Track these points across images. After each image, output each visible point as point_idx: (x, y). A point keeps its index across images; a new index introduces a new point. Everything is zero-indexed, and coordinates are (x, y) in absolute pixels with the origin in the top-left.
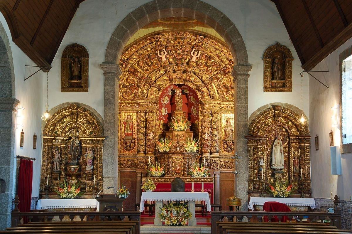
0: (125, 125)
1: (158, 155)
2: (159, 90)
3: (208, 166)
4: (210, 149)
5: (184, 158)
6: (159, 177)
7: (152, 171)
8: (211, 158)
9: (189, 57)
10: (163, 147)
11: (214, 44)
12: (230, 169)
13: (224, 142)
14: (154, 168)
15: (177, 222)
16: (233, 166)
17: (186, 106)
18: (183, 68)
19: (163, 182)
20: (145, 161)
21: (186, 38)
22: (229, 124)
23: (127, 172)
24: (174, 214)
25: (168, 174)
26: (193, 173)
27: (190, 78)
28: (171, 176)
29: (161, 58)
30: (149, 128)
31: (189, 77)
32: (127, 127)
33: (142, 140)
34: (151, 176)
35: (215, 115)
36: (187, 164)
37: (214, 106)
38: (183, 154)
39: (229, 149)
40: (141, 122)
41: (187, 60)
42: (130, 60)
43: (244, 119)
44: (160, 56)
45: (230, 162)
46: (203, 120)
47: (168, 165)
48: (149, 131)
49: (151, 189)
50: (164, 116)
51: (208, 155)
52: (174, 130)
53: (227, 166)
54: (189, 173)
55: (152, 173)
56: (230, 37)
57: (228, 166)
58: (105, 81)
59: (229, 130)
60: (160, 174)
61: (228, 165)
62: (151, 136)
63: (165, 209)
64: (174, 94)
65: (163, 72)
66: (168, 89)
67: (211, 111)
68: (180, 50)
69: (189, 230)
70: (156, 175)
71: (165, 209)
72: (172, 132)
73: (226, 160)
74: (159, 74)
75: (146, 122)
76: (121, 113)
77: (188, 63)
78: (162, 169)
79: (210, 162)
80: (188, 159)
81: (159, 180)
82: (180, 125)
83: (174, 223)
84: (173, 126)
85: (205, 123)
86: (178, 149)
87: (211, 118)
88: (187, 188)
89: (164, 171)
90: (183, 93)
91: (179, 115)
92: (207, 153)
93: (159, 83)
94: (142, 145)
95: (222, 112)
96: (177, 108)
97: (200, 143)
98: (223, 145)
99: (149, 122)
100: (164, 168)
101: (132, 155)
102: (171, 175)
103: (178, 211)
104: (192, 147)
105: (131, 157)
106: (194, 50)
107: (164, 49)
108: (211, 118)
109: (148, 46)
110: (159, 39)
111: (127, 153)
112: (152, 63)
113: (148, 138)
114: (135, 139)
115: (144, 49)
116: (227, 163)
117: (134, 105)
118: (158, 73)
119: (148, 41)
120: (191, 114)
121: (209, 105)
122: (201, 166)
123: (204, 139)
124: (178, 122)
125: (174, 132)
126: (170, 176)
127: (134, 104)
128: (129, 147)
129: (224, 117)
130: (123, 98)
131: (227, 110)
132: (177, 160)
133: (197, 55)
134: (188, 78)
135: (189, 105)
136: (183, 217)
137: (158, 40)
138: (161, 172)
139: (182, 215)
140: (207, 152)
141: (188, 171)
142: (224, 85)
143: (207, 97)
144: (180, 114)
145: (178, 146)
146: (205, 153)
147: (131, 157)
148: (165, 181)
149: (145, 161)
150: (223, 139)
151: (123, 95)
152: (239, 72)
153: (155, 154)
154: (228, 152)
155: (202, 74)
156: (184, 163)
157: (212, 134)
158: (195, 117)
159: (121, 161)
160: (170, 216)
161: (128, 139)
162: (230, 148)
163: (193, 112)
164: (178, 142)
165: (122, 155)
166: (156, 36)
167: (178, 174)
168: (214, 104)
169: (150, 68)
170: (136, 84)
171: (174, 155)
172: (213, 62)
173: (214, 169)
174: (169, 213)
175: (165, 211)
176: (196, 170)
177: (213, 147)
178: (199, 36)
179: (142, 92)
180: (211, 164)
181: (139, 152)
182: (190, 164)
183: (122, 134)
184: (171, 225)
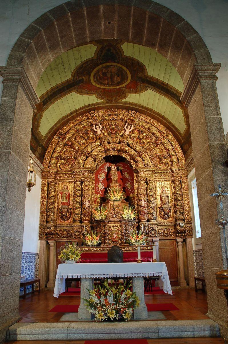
0: (61, 194)
1: (95, 225)
2: (95, 161)
3: (147, 234)
4: (147, 216)
5: (121, 226)
6: (95, 246)
7: (88, 240)
8: (149, 225)
9: (123, 132)
10: (99, 216)
11: (146, 119)
12: (168, 237)
13: (161, 209)
14: (90, 237)
15: (116, 314)
16: (170, 233)
17: (121, 181)
18: (117, 139)
19: (100, 252)
20: (80, 230)
21: (119, 114)
22: (164, 191)
23: (63, 242)
24: (111, 299)
25: (105, 243)
26: (131, 241)
27: (124, 148)
28: (107, 245)
29: (96, 132)
30: (84, 197)
31: (123, 147)
32: (63, 197)
33: (78, 209)
34: (87, 246)
35: (151, 183)
36: (124, 231)
37: (149, 174)
38: (120, 221)
39: (166, 216)
40: (77, 191)
41: (121, 134)
42: (67, 134)
43: (219, 137)
44: (95, 130)
45: (168, 230)
46: (138, 188)
47: (104, 234)
48: (85, 199)
49: (72, 260)
50: (101, 190)
51: (145, 222)
52: (110, 200)
53: (165, 233)
54: (127, 241)
55: (87, 242)
56: (183, 33)
57: (166, 234)
58: (3, 90)
59: (165, 196)
60: (95, 243)
61: (166, 232)
62: (87, 204)
63: (96, 291)
64: (109, 170)
65: (98, 144)
66: (104, 166)
67: (146, 179)
68: (114, 125)
69: (136, 331)
70: (92, 244)
71: (96, 291)
72: (108, 202)
73: (164, 228)
74: (95, 146)
75: (82, 191)
76: (58, 183)
77: (122, 136)
78: (98, 238)
79: (148, 230)
80: (125, 226)
81: (95, 249)
82: (116, 195)
83: (111, 316)
84: (110, 196)
85: (140, 190)
86: (115, 216)
87: (146, 186)
88: (131, 257)
89: (100, 239)
90: (118, 169)
91: (115, 187)
92: (144, 221)
93: (94, 153)
94: (77, 214)
95: (157, 180)
96: (113, 181)
97: (136, 212)
98: (160, 212)
99: (85, 191)
100: (100, 237)
101: (68, 225)
102: (107, 244)
103: (116, 294)
104: (129, 214)
105: (68, 227)
106: (127, 124)
107: (99, 124)
108: (146, 186)
109: (84, 122)
110: (94, 115)
111: (64, 223)
112: (88, 137)
113: (84, 206)
114: (71, 209)
115: (80, 124)
116: (165, 230)
117: (71, 176)
118: (94, 145)
119: (84, 117)
120: (125, 188)
121: (144, 173)
122: (139, 233)
123: (141, 206)
124: (114, 193)
125: (110, 202)
126: (106, 246)
127: (71, 175)
128: (64, 217)
129: (159, 185)
130: (61, 169)
131: (162, 178)
132: (114, 228)
133: (130, 129)
134: (122, 148)
135: (123, 180)
136: (125, 305)
137: (93, 115)
138: (97, 241)
139: (124, 301)
140: (144, 219)
141: (126, 240)
142: (157, 156)
143: (141, 165)
144: (115, 186)
145: (114, 213)
146: (142, 220)
147: (68, 227)
148: (101, 251)
149: (80, 230)
150: (160, 206)
151: (60, 167)
152: (202, 73)
153: (91, 223)
154: (165, 219)
155: (136, 144)
156: (121, 231)
157: (149, 202)
158: (130, 191)
159: (57, 231)
160: (104, 304)
161: (64, 209)
162: (167, 215)
163: (127, 187)
164: (114, 209)
165: (58, 225)
166: (92, 112)
167: (115, 243)
168: (149, 172)
169: (87, 142)
170: (73, 157)
171: (110, 222)
172: (145, 135)
173: (152, 237)
174: (102, 298)
175: (96, 295)
176: (134, 238)
177: (150, 214)
178: (132, 111)
179: (78, 163)
180: (149, 231)
181: (75, 221)
182: (127, 232)
183: (59, 204)
184: (105, 321)
